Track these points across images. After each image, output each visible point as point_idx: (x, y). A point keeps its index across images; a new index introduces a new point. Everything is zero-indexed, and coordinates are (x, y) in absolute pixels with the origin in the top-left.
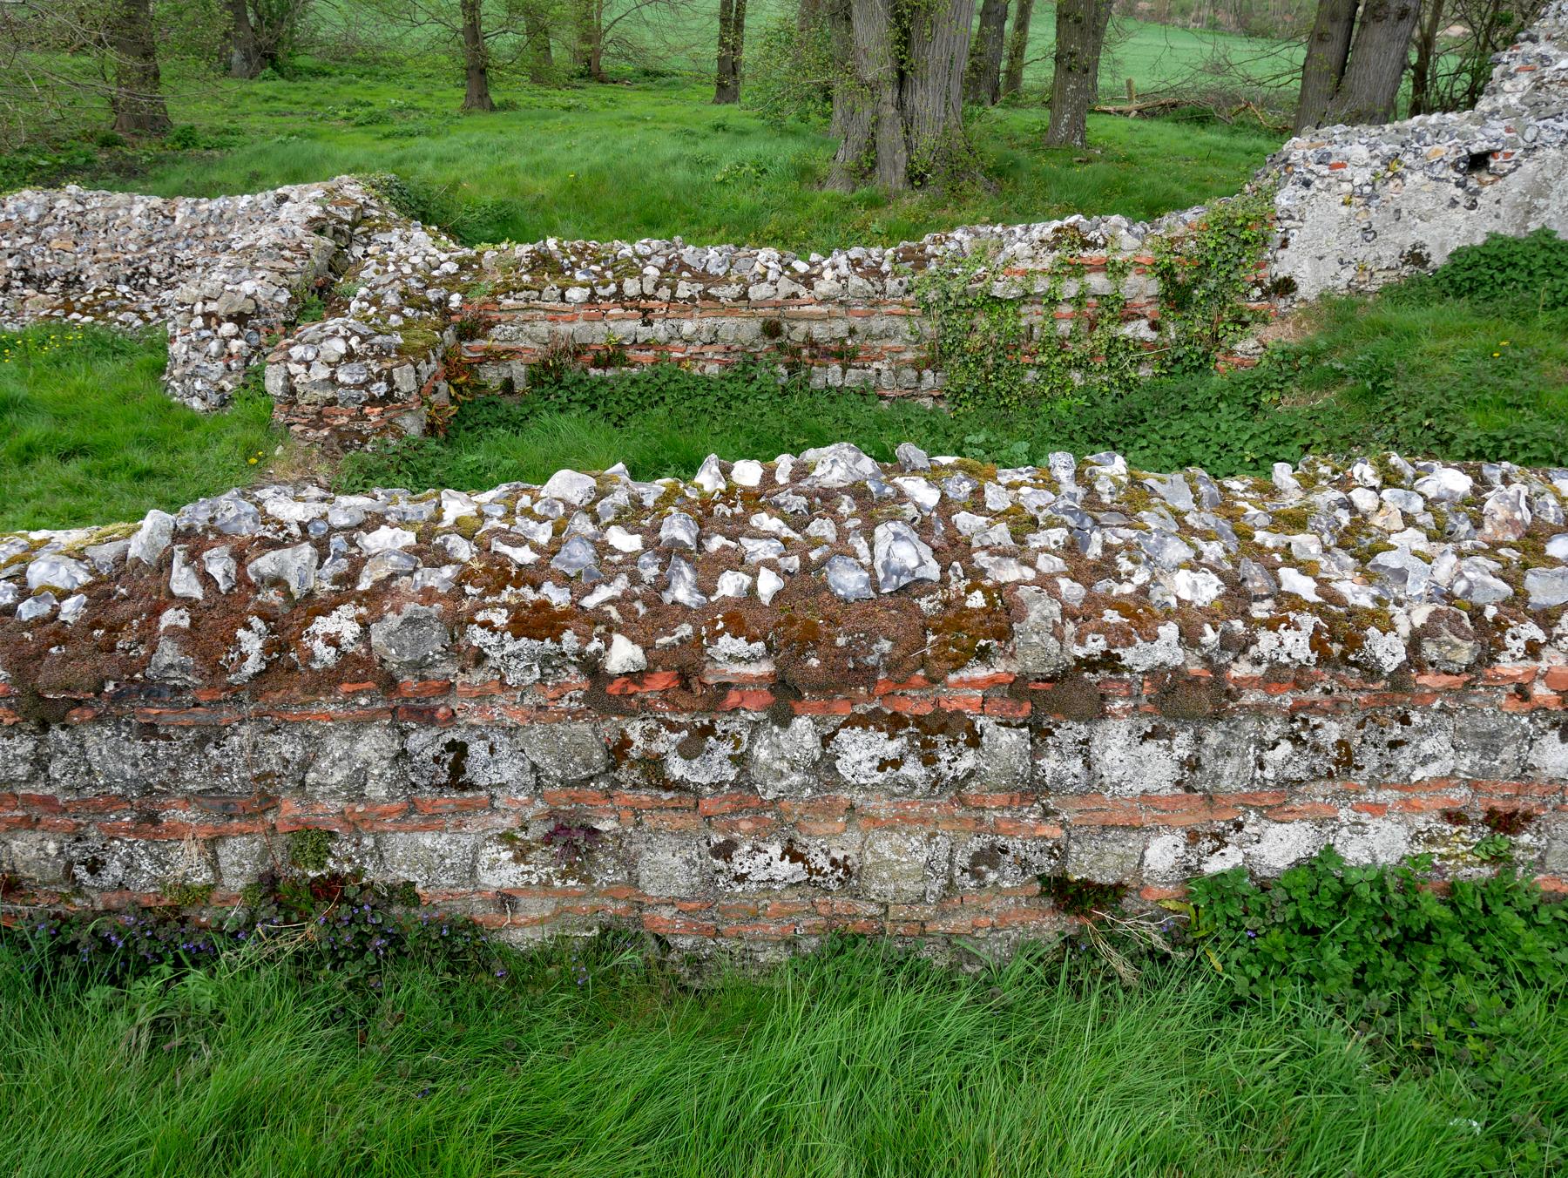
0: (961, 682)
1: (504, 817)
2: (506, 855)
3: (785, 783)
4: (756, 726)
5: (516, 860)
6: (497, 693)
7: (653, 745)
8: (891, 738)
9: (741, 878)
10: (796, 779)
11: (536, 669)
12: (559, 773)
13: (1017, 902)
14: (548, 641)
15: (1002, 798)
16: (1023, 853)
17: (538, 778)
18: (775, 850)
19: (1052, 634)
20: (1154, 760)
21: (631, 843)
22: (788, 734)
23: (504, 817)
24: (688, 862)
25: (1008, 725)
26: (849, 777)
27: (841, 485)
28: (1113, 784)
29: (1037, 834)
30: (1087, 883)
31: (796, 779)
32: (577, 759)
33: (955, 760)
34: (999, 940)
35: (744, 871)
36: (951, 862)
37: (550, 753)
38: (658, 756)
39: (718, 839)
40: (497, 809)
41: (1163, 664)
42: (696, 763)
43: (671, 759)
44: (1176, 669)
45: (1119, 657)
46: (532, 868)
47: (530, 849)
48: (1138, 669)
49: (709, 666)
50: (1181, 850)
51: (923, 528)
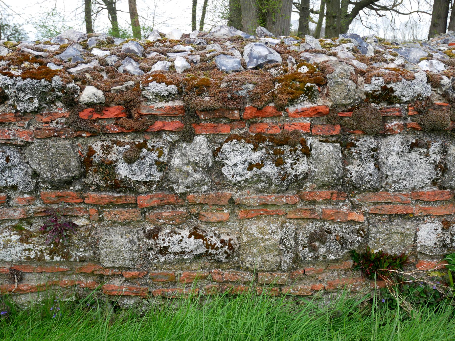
0: (298, 113)
1: (15, 211)
2: (15, 238)
3: (190, 179)
4: (173, 145)
5: (21, 241)
6: (13, 121)
7: (109, 156)
8: (255, 150)
9: (164, 251)
10: (197, 176)
11: (36, 100)
12: (49, 175)
13: (339, 275)
14: (43, 80)
15: (325, 193)
16: (341, 233)
17: (37, 183)
18: (185, 232)
19: (350, 79)
20: (418, 164)
21: (96, 233)
23: (15, 211)
24: (130, 241)
26: (230, 178)
27: (226, 37)
28: (394, 182)
29: (349, 218)
30: (381, 254)
31: (197, 176)
32: (61, 166)
33: (295, 164)
34: (329, 299)
36: (296, 239)
37: (43, 160)
38: (111, 162)
39: (149, 227)
40: (11, 206)
41: (419, 95)
42: (134, 166)
43: (119, 165)
44: (428, 98)
45: (392, 90)
46: (31, 246)
47: (32, 236)
48: (405, 99)
49: (143, 104)
50: (440, 231)
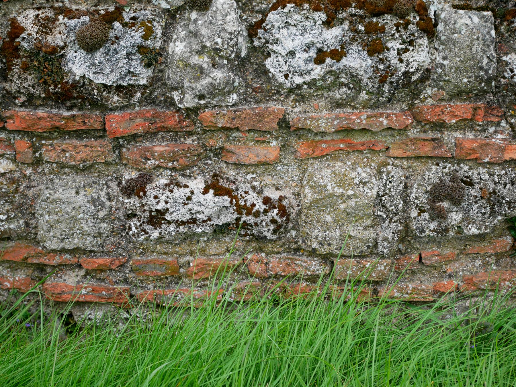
3: (205, 81)
7: (49, 38)
8: (328, 24)
16: (491, 185)
21: (29, 187)
22: (208, 16)
24: (93, 201)
25: (467, 7)
26: (281, 79)
33: (406, 50)
35: (160, 206)
43: (70, 54)
51: (509, 281)
